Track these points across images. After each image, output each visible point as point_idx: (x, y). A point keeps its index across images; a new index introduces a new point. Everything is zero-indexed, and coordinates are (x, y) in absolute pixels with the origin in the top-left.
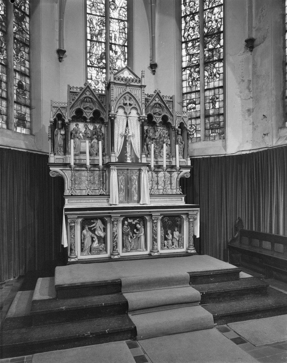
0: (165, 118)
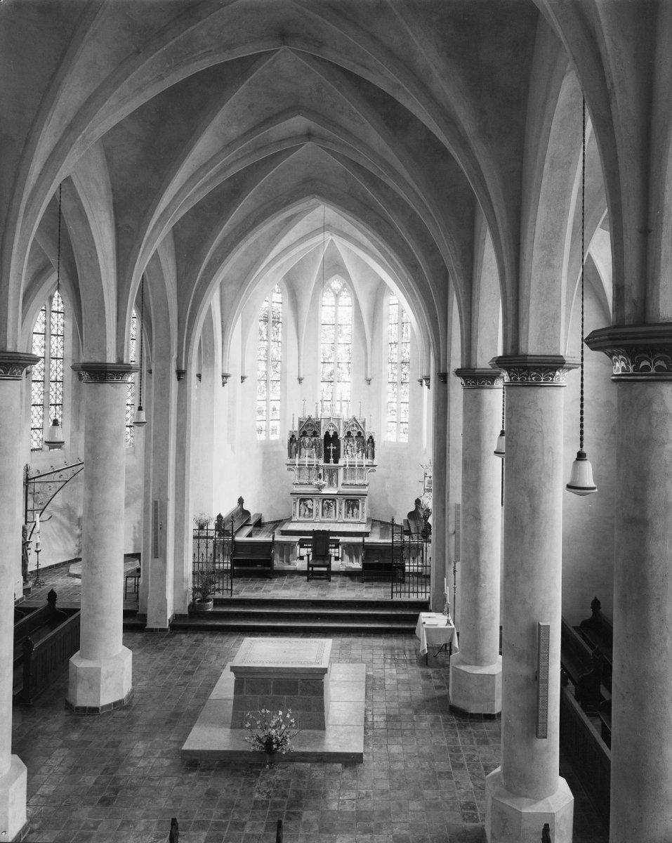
0: (359, 433)
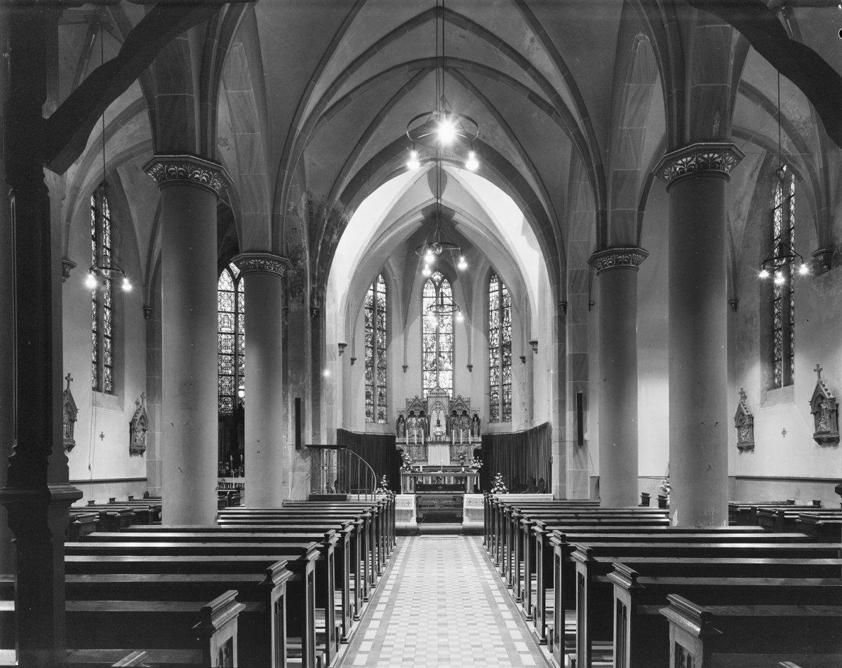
0: (465, 413)
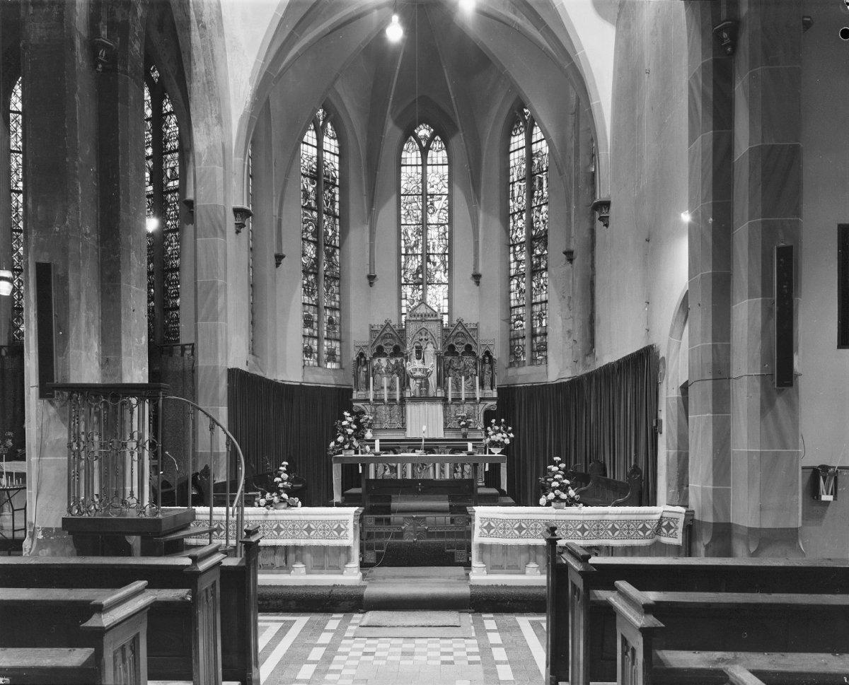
0: (469, 348)
